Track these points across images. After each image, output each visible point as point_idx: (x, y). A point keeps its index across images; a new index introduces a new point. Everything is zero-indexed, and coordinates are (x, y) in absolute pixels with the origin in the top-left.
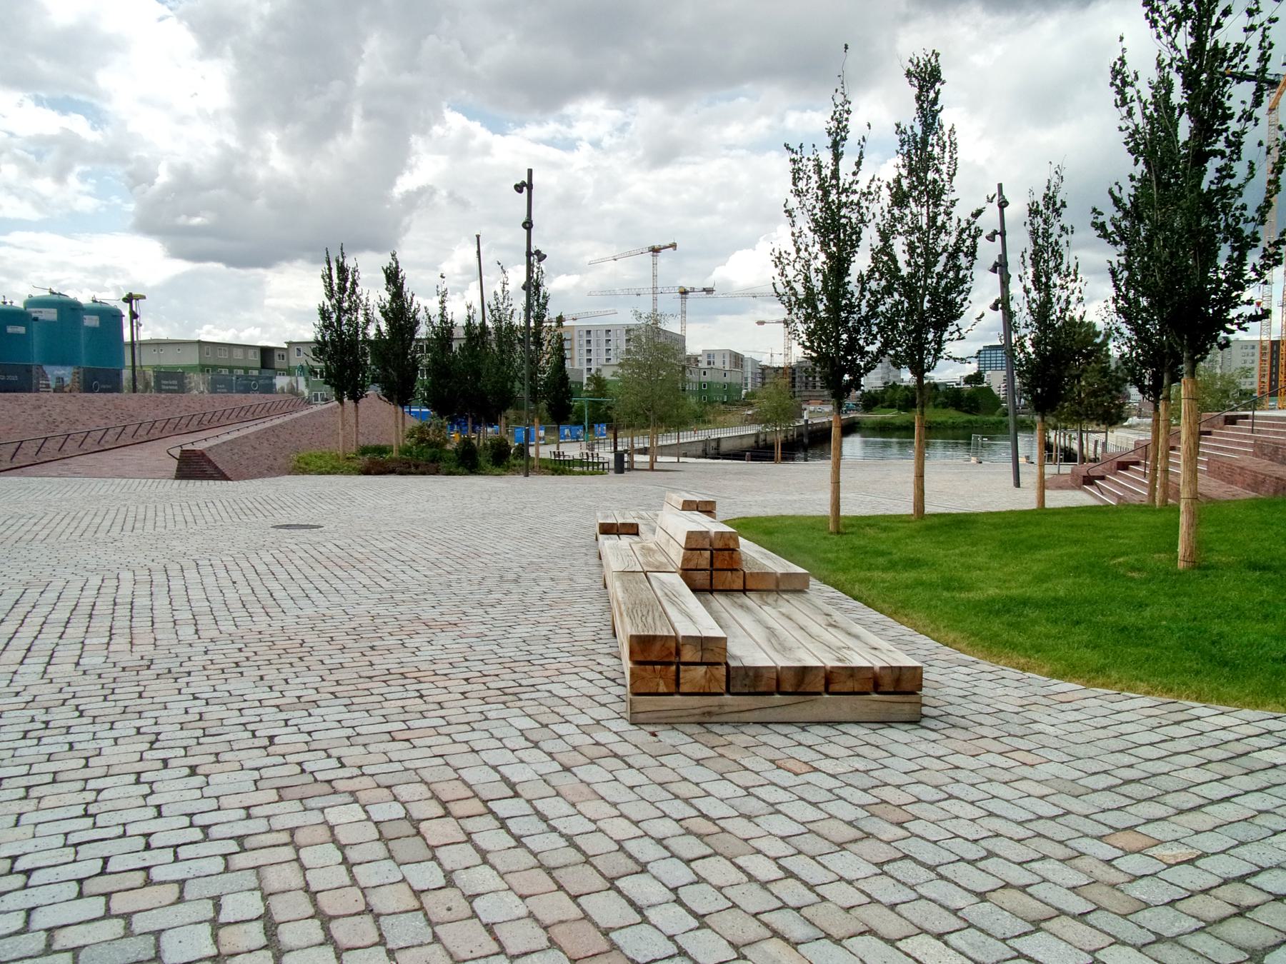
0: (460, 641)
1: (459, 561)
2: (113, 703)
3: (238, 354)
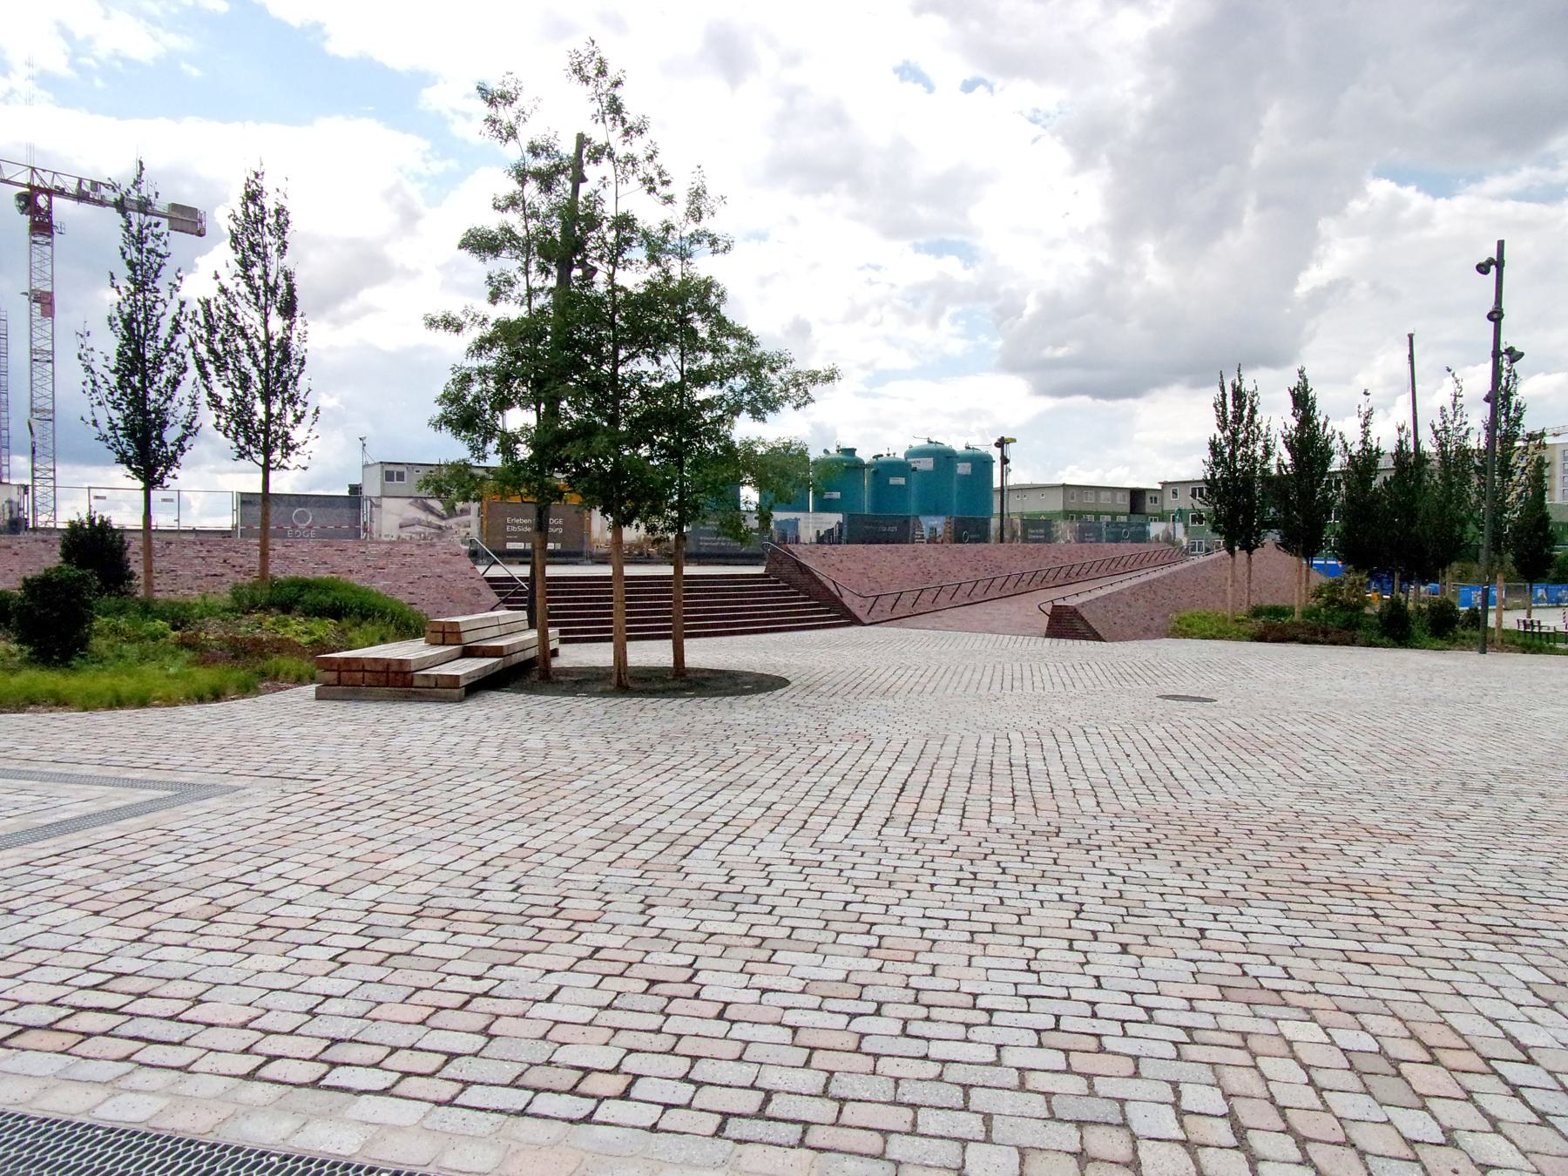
0: (1418, 857)
1: (1399, 757)
2: (1031, 866)
3: (1090, 498)
